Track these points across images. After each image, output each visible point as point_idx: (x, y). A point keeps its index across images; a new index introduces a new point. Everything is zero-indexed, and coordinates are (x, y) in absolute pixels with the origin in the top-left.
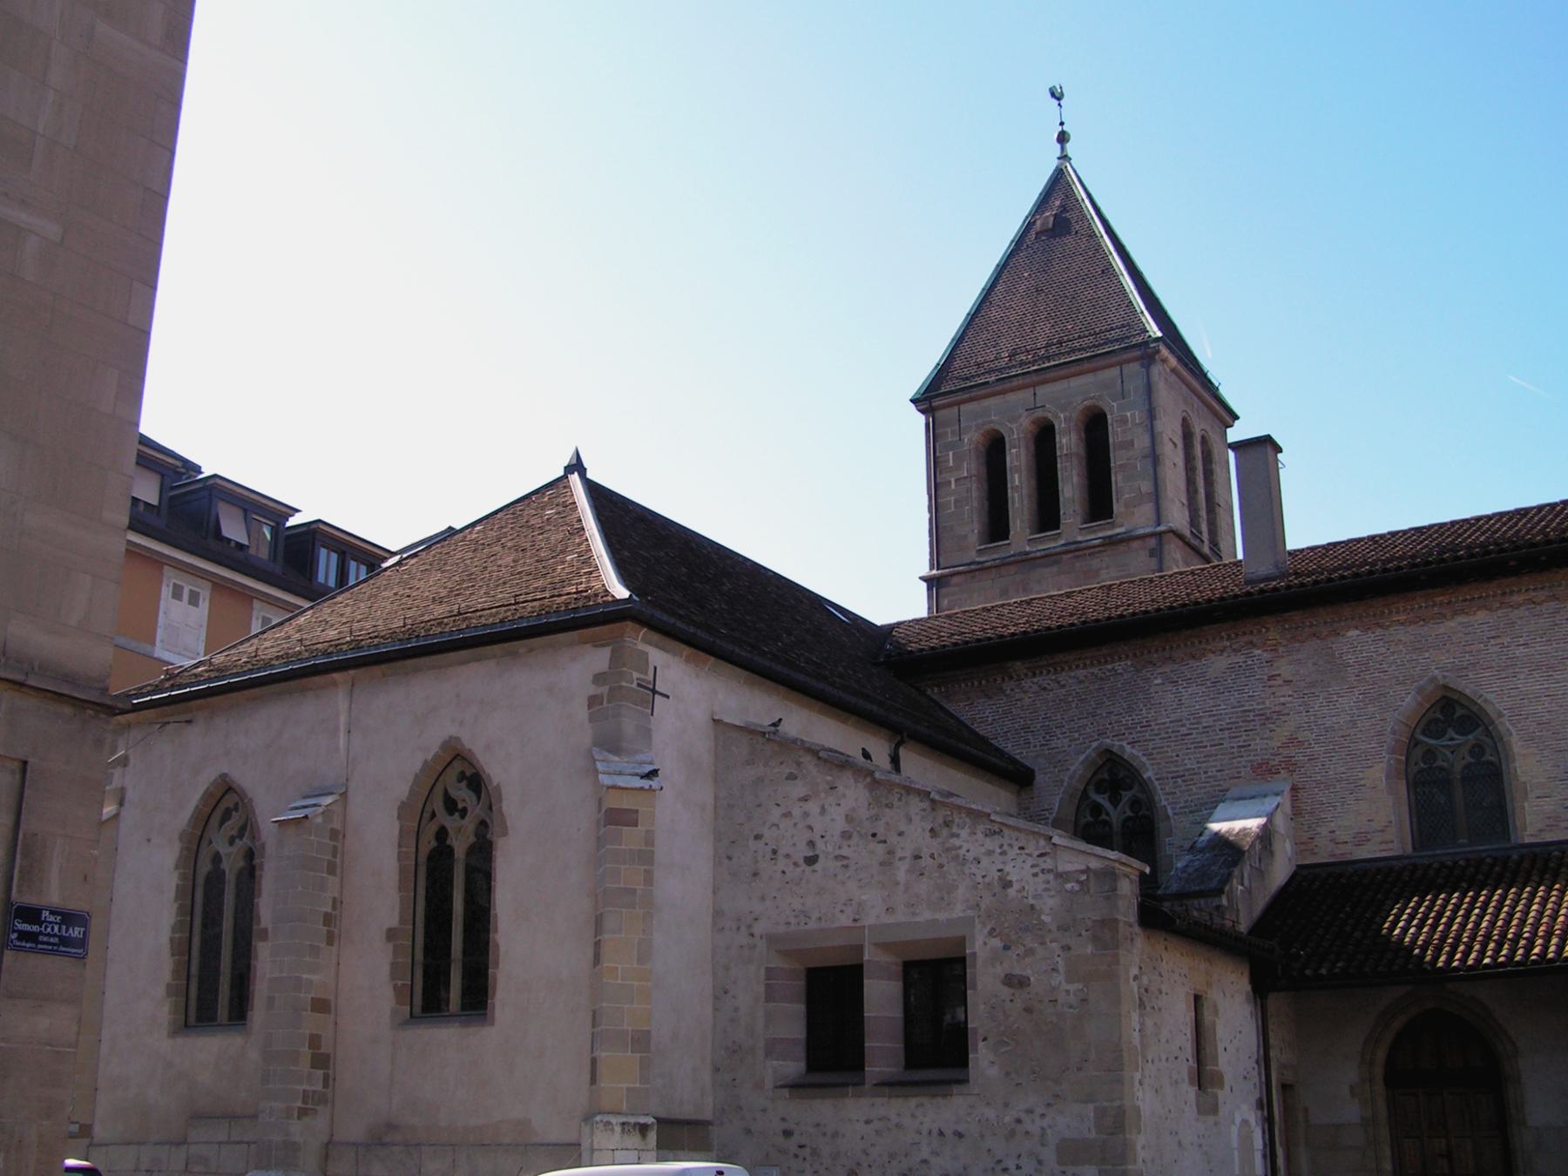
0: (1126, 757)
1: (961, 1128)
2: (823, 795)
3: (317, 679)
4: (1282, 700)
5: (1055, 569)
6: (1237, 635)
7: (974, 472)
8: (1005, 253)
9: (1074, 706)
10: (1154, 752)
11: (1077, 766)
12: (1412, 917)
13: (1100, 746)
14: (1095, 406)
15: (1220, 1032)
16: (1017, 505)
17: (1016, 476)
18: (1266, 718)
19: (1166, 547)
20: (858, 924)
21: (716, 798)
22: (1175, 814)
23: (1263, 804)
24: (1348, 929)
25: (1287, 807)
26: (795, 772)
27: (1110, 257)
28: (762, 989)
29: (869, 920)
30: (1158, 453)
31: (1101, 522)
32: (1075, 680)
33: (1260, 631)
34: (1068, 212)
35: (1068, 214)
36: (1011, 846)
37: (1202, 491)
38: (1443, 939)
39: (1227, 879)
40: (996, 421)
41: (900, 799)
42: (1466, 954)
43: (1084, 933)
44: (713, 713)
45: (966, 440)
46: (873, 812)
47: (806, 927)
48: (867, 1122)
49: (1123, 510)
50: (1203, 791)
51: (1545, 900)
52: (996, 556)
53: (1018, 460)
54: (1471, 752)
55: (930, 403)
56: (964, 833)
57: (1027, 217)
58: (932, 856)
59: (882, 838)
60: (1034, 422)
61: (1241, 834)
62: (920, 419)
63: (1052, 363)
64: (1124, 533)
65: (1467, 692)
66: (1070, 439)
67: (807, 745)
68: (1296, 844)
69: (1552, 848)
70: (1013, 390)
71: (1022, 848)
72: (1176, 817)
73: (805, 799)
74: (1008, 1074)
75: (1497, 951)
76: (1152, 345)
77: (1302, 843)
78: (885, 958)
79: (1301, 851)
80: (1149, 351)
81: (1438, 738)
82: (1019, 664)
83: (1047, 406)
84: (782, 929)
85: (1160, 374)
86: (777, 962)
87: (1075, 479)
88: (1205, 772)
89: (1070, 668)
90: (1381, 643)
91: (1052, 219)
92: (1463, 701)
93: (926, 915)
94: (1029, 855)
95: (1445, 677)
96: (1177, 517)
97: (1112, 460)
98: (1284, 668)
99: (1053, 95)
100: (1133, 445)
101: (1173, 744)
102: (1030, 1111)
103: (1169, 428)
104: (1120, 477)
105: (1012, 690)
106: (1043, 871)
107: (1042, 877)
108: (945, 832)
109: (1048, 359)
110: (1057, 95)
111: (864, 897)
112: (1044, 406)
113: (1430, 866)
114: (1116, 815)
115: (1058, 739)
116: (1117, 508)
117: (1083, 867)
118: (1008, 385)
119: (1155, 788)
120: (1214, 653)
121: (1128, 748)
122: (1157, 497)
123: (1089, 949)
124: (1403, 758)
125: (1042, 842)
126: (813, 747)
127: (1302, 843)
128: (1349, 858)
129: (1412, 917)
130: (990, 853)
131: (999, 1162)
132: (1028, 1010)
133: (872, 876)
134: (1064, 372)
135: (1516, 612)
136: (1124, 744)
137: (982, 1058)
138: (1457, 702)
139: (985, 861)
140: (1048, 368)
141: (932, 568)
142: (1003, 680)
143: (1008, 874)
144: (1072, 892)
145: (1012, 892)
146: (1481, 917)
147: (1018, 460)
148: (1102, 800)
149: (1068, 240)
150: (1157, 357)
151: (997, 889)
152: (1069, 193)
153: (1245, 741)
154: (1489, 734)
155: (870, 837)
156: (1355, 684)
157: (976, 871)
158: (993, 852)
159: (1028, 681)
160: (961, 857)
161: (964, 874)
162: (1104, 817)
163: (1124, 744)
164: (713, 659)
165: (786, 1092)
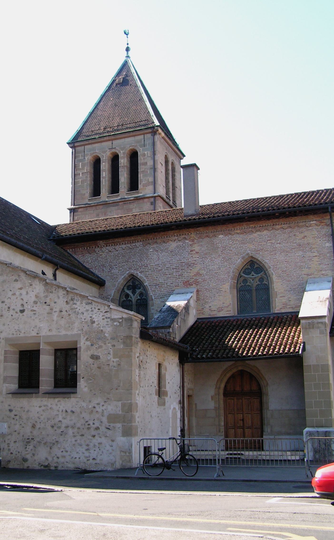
1: (74, 409)
2: (27, 288)
4: (195, 259)
5: (116, 208)
9: (121, 257)
11: (121, 280)
16: (104, 184)
19: (157, 202)
23: (186, 296)
25: (195, 298)
27: (142, 95)
30: (156, 167)
31: (134, 191)
36: (95, 308)
38: (246, 346)
39: (172, 322)
41: (55, 290)
42: (253, 351)
43: (120, 340)
46: (45, 294)
47: (20, 336)
51: (280, 333)
52: (95, 202)
53: (105, 167)
54: (259, 280)
55: (74, 144)
56: (78, 303)
58: (66, 311)
59: (49, 304)
63: (119, 132)
65: (259, 259)
67: (22, 269)
69: (284, 315)
71: (99, 309)
73: (21, 289)
74: (91, 390)
75: (264, 350)
76: (156, 128)
78: (48, 348)
80: (154, 130)
81: (248, 275)
84: (10, 336)
85: (158, 138)
86: (9, 348)
87: (125, 175)
89: (120, 244)
91: (122, 79)
92: (258, 262)
93: (63, 332)
95: (252, 253)
96: (161, 191)
97: (139, 169)
98: (196, 248)
99: (125, 33)
100: (147, 164)
101: (155, 273)
102: (98, 404)
103: (160, 159)
104: (141, 176)
107: (106, 320)
108: (71, 302)
109: (118, 130)
110: (126, 33)
116: (140, 186)
117: (121, 317)
118: (102, 140)
119: (148, 289)
121: (139, 274)
122: (154, 183)
123: (122, 346)
124: (236, 282)
125: (106, 307)
128: (215, 316)
129: (236, 338)
130: (87, 310)
131: (87, 422)
132: (99, 368)
135: (277, 231)
136: (138, 272)
137: (82, 384)
139: (85, 314)
140: (118, 134)
141: (72, 205)
143: (93, 318)
144: (116, 326)
145: (95, 325)
147: (105, 167)
148: (130, 292)
149: (128, 87)
150: (157, 132)
151: (89, 324)
152: (129, 70)
153: (181, 273)
154: (266, 274)
162: (129, 298)
163: (138, 272)
165: (10, 395)
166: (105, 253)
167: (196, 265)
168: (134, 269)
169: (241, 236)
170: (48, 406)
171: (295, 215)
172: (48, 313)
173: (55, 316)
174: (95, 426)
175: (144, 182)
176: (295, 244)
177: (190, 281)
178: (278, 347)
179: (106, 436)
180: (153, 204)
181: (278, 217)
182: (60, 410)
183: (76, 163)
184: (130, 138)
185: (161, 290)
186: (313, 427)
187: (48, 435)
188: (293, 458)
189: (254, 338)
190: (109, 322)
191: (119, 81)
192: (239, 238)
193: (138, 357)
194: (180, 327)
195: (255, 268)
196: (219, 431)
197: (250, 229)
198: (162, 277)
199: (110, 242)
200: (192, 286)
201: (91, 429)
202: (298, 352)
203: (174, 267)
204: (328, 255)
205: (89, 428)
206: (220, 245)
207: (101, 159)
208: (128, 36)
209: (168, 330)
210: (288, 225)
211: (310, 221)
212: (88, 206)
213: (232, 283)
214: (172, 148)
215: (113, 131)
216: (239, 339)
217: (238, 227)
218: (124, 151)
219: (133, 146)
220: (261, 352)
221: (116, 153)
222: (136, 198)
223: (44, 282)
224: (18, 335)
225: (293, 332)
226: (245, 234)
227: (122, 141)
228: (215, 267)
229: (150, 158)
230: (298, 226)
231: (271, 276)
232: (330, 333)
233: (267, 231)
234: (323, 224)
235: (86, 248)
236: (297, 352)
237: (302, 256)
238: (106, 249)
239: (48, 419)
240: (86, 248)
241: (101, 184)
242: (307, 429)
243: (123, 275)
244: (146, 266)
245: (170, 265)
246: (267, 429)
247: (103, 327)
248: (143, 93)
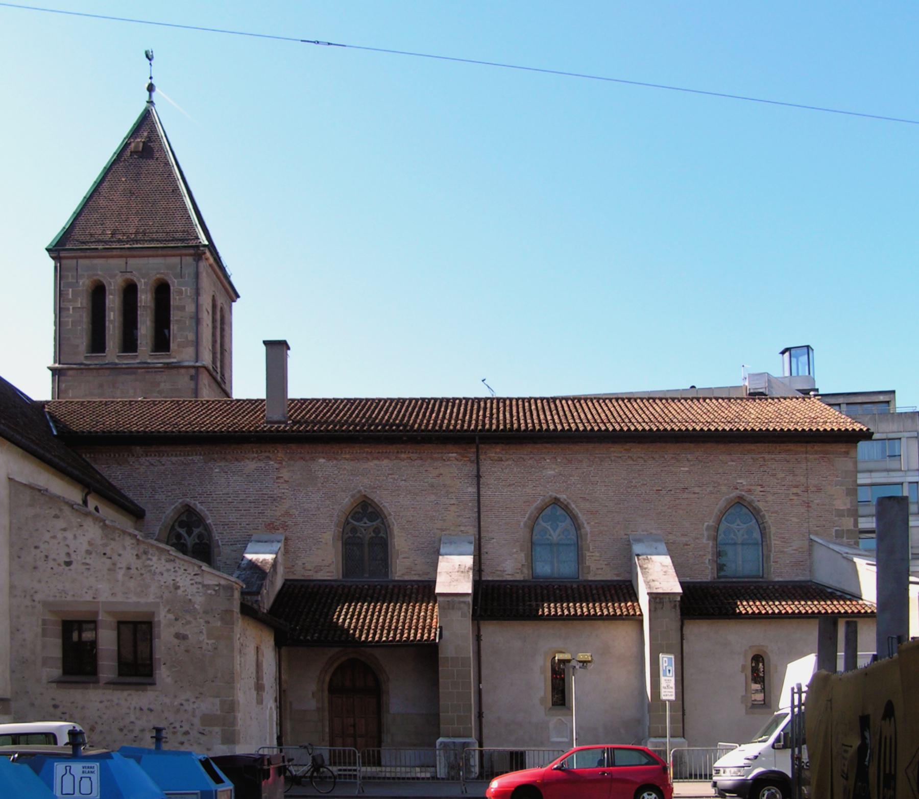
0: (197, 510)
1: (151, 707)
2: (75, 529)
4: (283, 491)
6: (261, 452)
7: (85, 305)
8: (109, 161)
9: (169, 476)
10: (213, 509)
11: (170, 512)
12: (347, 613)
13: (184, 501)
14: (163, 279)
15: (264, 664)
16: (111, 332)
17: (112, 313)
18: (274, 499)
19: (200, 376)
20: (96, 600)
21: (11, 523)
22: (223, 545)
23: (272, 547)
24: (317, 617)
25: (282, 549)
26: (59, 514)
27: (178, 182)
28: (39, 630)
29: (102, 598)
30: (200, 317)
31: (163, 353)
32: (170, 463)
33: (274, 452)
34: (152, 142)
35: (152, 144)
36: (179, 568)
37: (219, 342)
38: (363, 626)
39: (261, 586)
40: (101, 275)
41: (119, 536)
42: (374, 634)
43: (216, 615)
44: (8, 474)
45: (81, 283)
46: (104, 541)
47: (65, 599)
48: (101, 702)
49: (176, 348)
50: (239, 534)
51: (407, 610)
52: (96, 362)
53: (113, 302)
54: (374, 531)
55: (59, 254)
56: (155, 559)
57: (125, 139)
58: (137, 569)
59: (109, 556)
60: (124, 281)
61: (264, 562)
62: (51, 263)
63: (139, 246)
64: (176, 363)
65: (375, 500)
66: (147, 297)
67: (67, 501)
68: (285, 568)
69: (407, 584)
70: (112, 257)
71: (185, 570)
72: (224, 546)
73: (65, 530)
74: (176, 682)
75: (388, 634)
76: (202, 249)
77: (288, 568)
78: (109, 619)
79: (288, 572)
80: (200, 252)
81: (355, 521)
82: (138, 448)
83: (134, 272)
84: (51, 599)
85: (204, 266)
86: (48, 617)
87: (149, 323)
88: (240, 524)
89: (168, 455)
90: (336, 468)
91: (141, 145)
92: (373, 505)
93: (133, 599)
94: (189, 574)
95: (365, 491)
96: (206, 359)
97: (172, 316)
98: (285, 474)
99: (147, 56)
100: (185, 309)
101: (223, 506)
102: (188, 700)
103: (206, 302)
104: (175, 328)
105: (133, 462)
106: (196, 583)
107: (195, 586)
108: (144, 557)
109: (137, 241)
110: (149, 57)
111: (100, 586)
112: (132, 272)
113: (351, 586)
114: (190, 541)
115: (160, 494)
116: (173, 346)
117: (217, 583)
119: (213, 529)
120: (248, 459)
121: (199, 505)
122: (197, 344)
123: (219, 624)
124: (341, 530)
125: (196, 568)
126: (70, 502)
127: (288, 568)
128: (311, 578)
129: (347, 613)
130: (168, 570)
131: (171, 724)
132: (187, 651)
133: (104, 576)
135: (403, 463)
136: (197, 502)
137: (163, 674)
138: (370, 504)
139: (165, 574)
140: (137, 248)
141: (55, 362)
142: (128, 455)
143: (178, 582)
144: (211, 594)
145: (180, 592)
146: (379, 616)
147: (113, 302)
148: (183, 532)
149: (151, 162)
150: (203, 256)
151: (172, 589)
152: (153, 130)
153: (262, 510)
154: (383, 523)
155: (102, 555)
156: (321, 488)
157: (161, 579)
158: (170, 570)
159: (144, 459)
160: (153, 571)
161: (154, 580)
162: (182, 541)
163: (197, 502)
164: (9, 443)
165: (54, 685)
166: (144, 467)
167: (285, 501)
168: (191, 498)
169: (352, 463)
170: (113, 701)
171: (430, 443)
172: (109, 570)
173: (120, 575)
174: (184, 729)
175: (179, 340)
176: (426, 484)
177: (275, 524)
178: (406, 631)
179: (200, 744)
180: (195, 378)
181: (404, 442)
182: (132, 707)
183: (62, 289)
184: (156, 258)
185: (232, 533)
186: (448, 736)
187: (115, 741)
188: (423, 775)
189: (372, 615)
190: (201, 589)
191: (136, 147)
192: (348, 466)
193: (239, 639)
194: (268, 592)
195: (368, 512)
196: (323, 740)
197: (365, 455)
198: (233, 513)
199: (153, 450)
200: (277, 531)
201: (178, 733)
202: (435, 639)
203: (252, 501)
204: (470, 504)
205: (174, 733)
206: (320, 474)
207: (107, 288)
208: (153, 62)
209: (255, 598)
210: (417, 455)
211: (448, 453)
212: (83, 369)
213: (336, 531)
214: (221, 283)
215: (128, 241)
216: (352, 616)
217: (347, 450)
218: (146, 280)
219: (162, 273)
220: (385, 637)
221: (132, 280)
222: (166, 366)
223: (101, 524)
224: (63, 599)
225: (423, 610)
226: (357, 461)
228: (312, 506)
229: (190, 300)
230: (432, 458)
231: (391, 527)
232: (472, 615)
233: (389, 461)
234: (465, 459)
235: (112, 456)
236: (433, 640)
237: (436, 502)
238: (146, 460)
239: (115, 719)
240: (112, 456)
241: (107, 331)
242: (441, 740)
243: (174, 504)
244: (208, 493)
245: (245, 496)
246: (387, 738)
247: (191, 595)
248: (178, 180)
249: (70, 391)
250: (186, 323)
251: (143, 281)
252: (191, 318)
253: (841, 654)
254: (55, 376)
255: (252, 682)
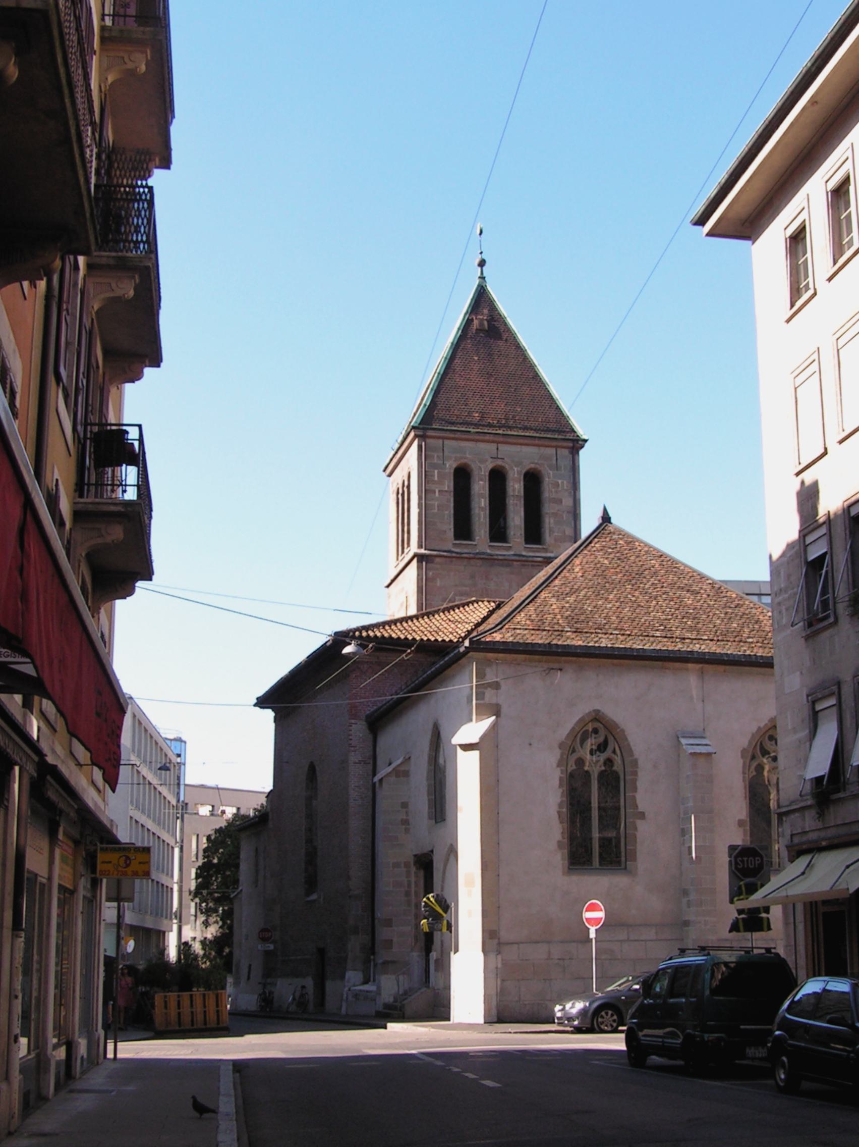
3: (678, 665)
5: (508, 569)
16: (482, 520)
34: (495, 321)
45: (448, 466)
49: (553, 542)
53: (480, 488)
63: (513, 433)
76: (580, 442)
100: (561, 502)
112: (503, 459)
118: (481, 437)
134: (521, 441)
147: (480, 488)
149: (500, 343)
175: (556, 534)
219: (536, 464)
227: (517, 448)
249: (438, 579)
250: (563, 518)
251: (516, 469)
252: (568, 512)
253: (37, 907)
254: (422, 563)
255: (848, 864)
